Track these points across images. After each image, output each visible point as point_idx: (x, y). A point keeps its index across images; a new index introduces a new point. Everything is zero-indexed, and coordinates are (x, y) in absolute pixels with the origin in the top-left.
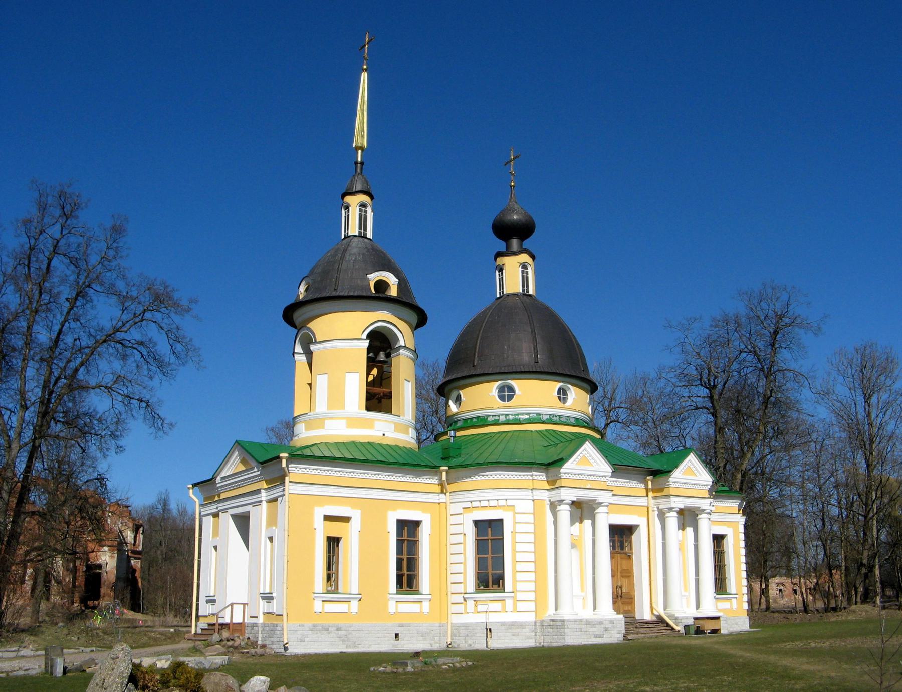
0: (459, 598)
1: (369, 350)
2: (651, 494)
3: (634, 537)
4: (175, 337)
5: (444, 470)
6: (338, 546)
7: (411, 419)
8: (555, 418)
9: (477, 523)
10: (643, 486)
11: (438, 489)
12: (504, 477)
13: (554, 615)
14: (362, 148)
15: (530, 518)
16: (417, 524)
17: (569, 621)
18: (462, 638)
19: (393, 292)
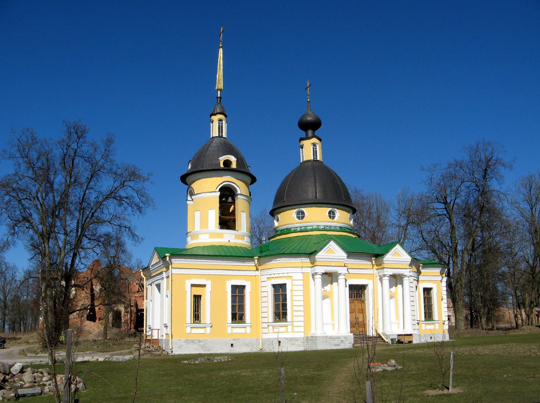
0: (265, 325)
1: (221, 197)
3: (366, 291)
4: (141, 194)
6: (200, 299)
7: (246, 231)
8: (327, 228)
9: (274, 286)
11: (255, 268)
12: (287, 261)
13: (403, 331)
14: (220, 90)
15: (301, 283)
16: (243, 287)
17: (319, 337)
18: (267, 346)
19: (234, 166)
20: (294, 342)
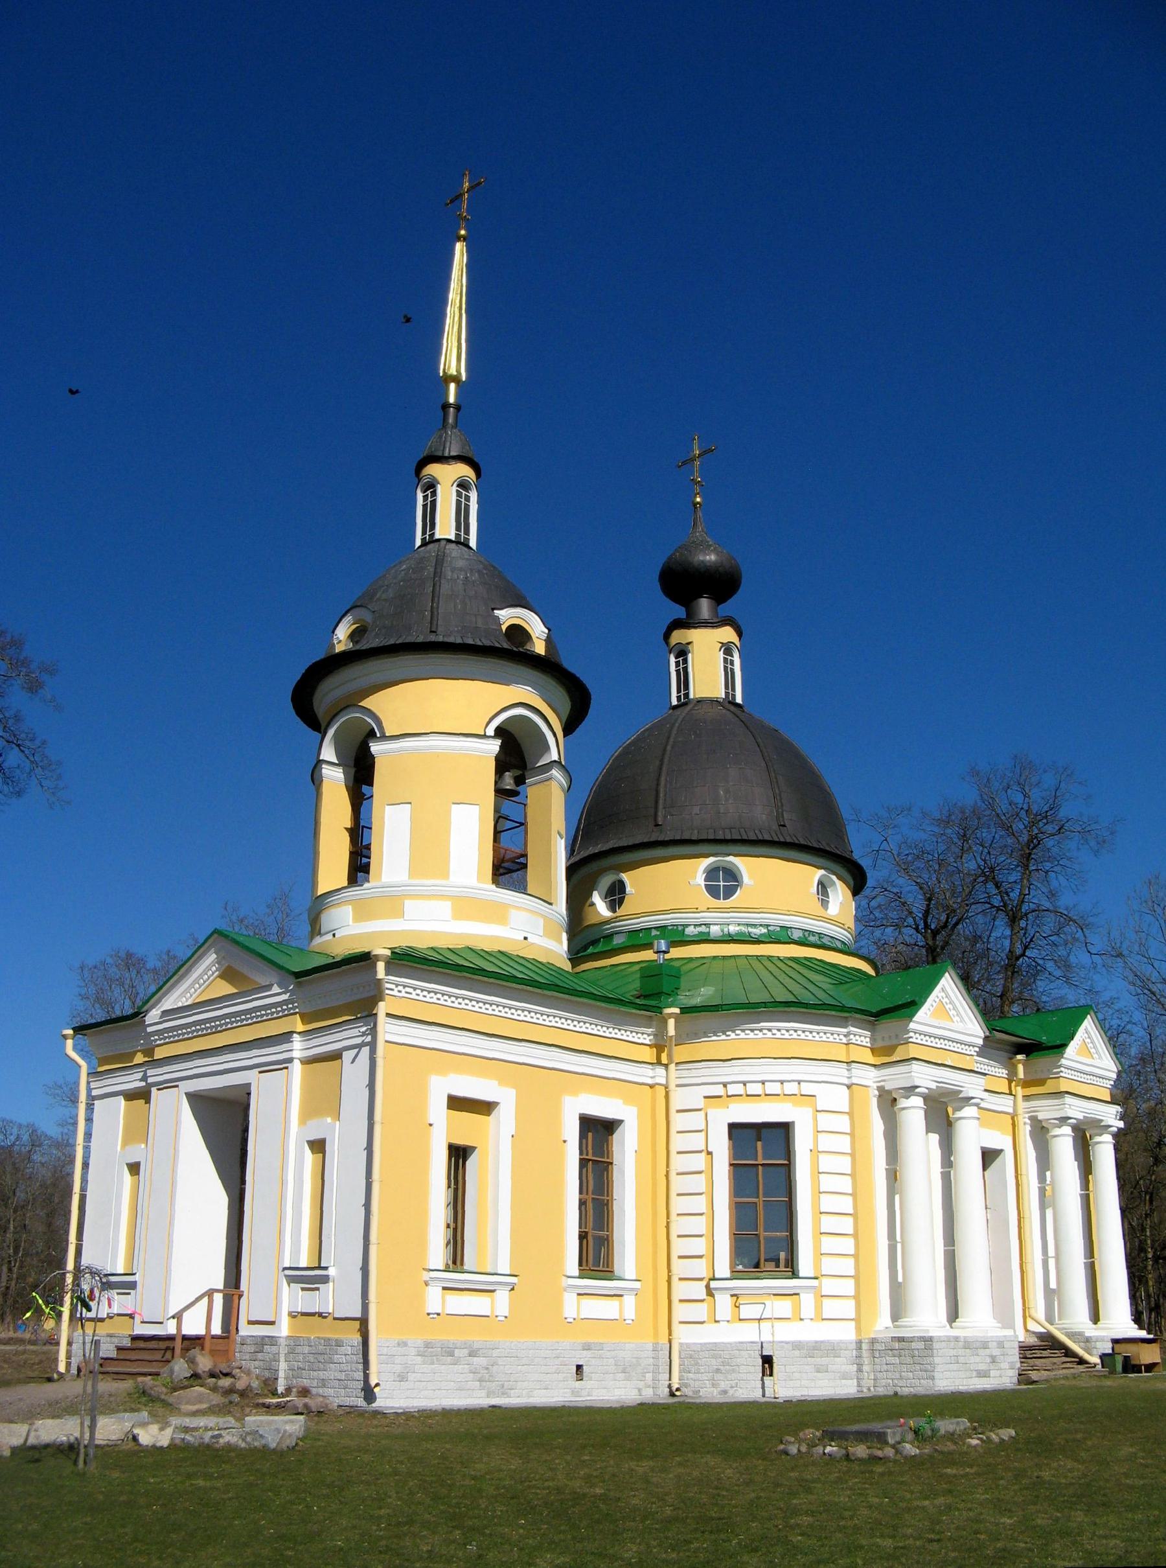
2: (1019, 1091)
5: (671, 1015)
10: (1003, 1072)
14: (456, 379)
19: (540, 648)
20: (825, 1361)
